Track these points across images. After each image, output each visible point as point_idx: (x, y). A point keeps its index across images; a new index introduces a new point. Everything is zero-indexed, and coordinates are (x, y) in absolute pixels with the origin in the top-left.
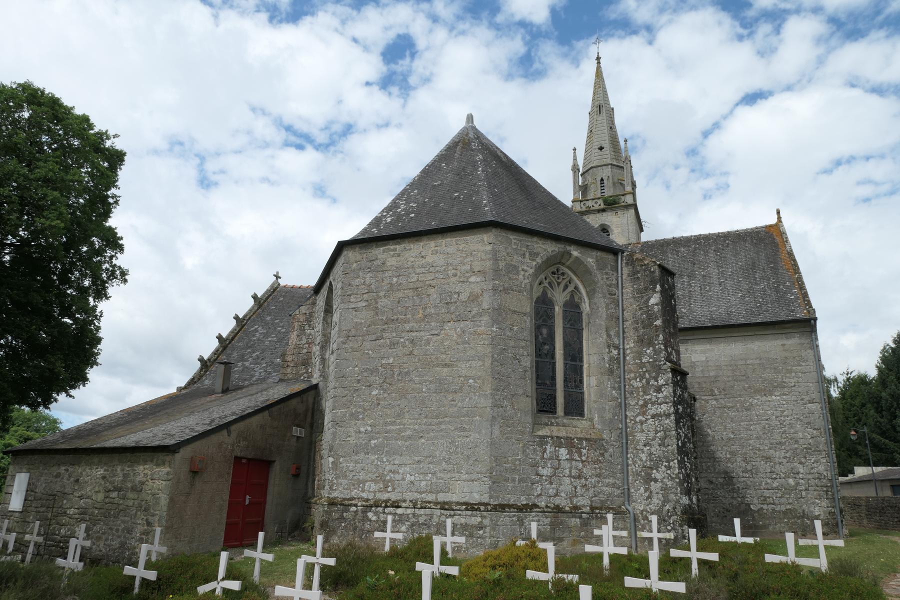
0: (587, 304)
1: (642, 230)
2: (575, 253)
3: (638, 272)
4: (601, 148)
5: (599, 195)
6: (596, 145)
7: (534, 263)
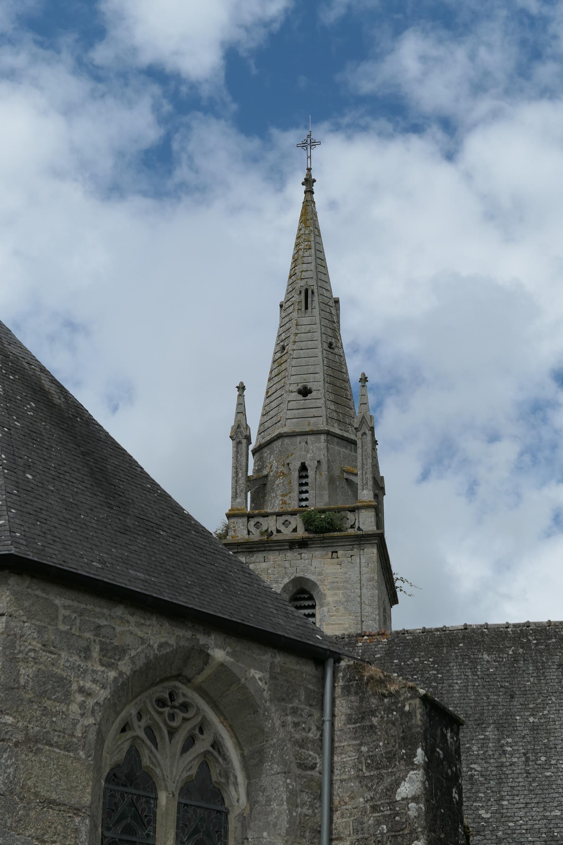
0: (242, 790)
1: (394, 600)
2: (219, 655)
3: (373, 713)
4: (305, 392)
5: (294, 505)
6: (294, 382)
7: (112, 674)
